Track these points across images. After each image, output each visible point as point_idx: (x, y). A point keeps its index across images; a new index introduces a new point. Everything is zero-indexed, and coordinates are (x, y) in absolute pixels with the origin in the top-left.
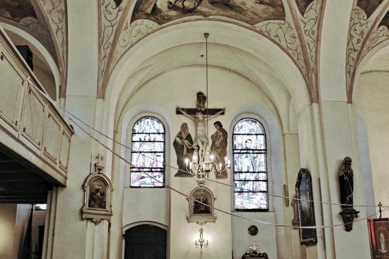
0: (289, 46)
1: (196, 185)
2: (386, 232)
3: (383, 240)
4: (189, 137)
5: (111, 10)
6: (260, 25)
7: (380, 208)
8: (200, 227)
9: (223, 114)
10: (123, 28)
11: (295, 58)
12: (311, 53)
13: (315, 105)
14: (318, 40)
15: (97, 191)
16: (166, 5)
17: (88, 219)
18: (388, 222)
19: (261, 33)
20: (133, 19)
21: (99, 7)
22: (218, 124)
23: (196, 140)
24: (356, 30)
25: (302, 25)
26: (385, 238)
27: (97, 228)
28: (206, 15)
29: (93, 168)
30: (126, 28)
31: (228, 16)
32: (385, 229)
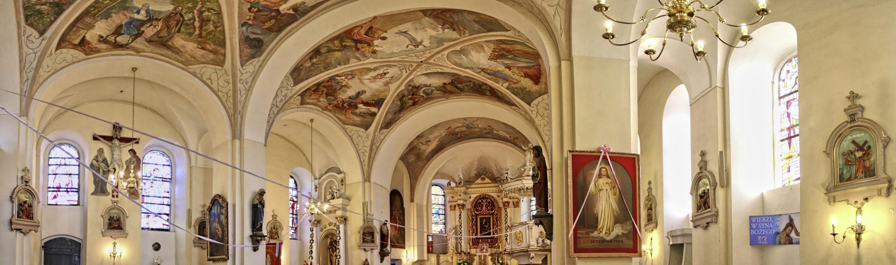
0: (221, 89)
1: (110, 204)
4: (105, 161)
5: (34, 39)
6: (192, 68)
8: (113, 241)
9: (137, 143)
10: (47, 55)
11: (224, 100)
12: (240, 98)
13: (237, 142)
14: (249, 90)
15: (25, 202)
16: (97, 38)
17: (17, 230)
19: (194, 74)
20: (57, 49)
21: (19, 37)
22: (132, 151)
23: (112, 163)
25: (239, 74)
27: (25, 238)
28: (138, 51)
29: (19, 180)
30: (51, 55)
31: (162, 55)
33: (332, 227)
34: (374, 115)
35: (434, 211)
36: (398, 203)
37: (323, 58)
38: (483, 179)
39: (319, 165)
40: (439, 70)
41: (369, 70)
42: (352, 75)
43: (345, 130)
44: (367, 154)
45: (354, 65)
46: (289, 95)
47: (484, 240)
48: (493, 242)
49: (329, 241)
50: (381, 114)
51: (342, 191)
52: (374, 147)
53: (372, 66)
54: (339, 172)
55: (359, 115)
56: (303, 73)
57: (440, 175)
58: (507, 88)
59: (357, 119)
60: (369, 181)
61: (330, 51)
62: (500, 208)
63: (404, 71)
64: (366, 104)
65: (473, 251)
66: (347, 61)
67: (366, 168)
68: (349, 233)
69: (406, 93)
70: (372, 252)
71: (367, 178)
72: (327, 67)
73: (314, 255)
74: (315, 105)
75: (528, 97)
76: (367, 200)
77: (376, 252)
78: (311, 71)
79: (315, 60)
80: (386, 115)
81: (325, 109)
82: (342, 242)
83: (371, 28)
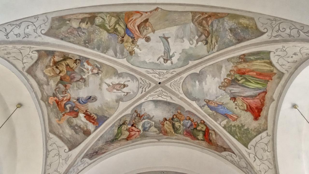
24: (28, 28)
34: (87, 133)
37: (91, 29)
40: (169, 100)
41: (116, 73)
42: (99, 68)
43: (46, 140)
45: (105, 58)
46: (31, 39)
50: (98, 134)
53: (120, 70)
55: (73, 127)
56: (64, 29)
58: (225, 127)
59: (68, 131)
61: (102, 26)
63: (140, 90)
64: (88, 116)
66: (105, 50)
69: (128, 120)
72: (87, 43)
74: (40, 85)
75: (245, 137)
78: (72, 33)
79: (83, 25)
80: (99, 140)
81: (45, 99)
83: (147, 20)
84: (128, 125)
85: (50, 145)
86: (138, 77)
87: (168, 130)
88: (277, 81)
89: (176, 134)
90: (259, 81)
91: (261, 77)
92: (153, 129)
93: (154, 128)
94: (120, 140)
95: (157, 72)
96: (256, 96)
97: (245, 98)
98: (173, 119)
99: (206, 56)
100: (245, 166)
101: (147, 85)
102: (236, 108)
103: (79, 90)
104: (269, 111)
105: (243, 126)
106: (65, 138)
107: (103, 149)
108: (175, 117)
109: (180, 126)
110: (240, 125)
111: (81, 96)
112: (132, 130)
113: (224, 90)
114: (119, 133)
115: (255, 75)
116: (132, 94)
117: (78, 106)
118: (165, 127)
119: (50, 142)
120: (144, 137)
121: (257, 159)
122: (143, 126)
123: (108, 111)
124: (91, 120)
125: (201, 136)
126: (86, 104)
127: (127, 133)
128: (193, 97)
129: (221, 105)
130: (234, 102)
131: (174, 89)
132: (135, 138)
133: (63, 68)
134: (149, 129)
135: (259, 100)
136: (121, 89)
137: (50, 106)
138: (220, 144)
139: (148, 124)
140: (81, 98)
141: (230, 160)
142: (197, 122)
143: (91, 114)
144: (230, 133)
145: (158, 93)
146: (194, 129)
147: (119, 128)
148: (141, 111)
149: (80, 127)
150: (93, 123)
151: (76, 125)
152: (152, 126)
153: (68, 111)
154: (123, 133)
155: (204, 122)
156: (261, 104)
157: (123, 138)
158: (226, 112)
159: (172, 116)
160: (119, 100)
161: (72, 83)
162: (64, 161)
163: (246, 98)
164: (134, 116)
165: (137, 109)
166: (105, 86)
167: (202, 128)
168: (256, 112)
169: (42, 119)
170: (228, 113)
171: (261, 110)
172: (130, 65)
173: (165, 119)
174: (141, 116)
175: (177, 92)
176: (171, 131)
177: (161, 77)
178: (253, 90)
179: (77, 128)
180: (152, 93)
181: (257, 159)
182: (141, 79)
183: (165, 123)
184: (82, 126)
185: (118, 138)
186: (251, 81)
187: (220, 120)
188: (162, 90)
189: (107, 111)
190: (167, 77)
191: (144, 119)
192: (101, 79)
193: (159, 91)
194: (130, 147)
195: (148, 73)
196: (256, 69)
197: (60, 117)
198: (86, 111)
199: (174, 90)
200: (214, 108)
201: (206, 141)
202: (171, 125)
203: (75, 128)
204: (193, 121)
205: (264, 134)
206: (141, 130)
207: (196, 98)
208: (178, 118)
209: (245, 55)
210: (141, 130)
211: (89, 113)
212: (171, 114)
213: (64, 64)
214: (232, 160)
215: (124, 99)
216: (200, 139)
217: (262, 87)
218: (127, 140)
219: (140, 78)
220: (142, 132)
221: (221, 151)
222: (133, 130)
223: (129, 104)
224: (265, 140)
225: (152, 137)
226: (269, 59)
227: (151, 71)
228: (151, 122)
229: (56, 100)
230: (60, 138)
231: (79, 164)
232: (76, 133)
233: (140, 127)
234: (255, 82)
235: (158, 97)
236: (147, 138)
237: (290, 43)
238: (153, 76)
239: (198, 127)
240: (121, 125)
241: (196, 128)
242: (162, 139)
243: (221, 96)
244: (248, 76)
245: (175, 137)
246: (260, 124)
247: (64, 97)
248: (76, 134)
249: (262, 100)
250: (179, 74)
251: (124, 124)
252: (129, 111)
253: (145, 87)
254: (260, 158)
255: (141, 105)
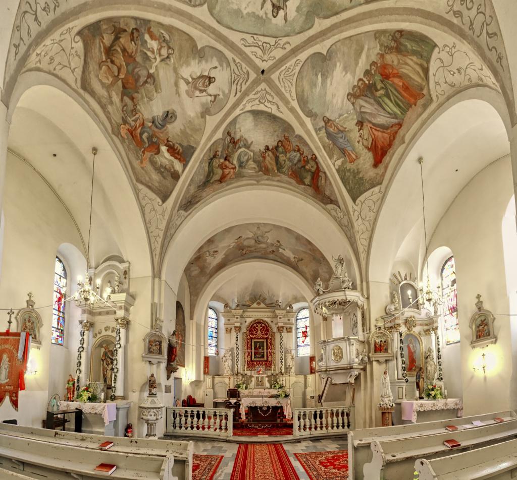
2: (13, 353)
3: (5, 365)
7: (10, 317)
18: (19, 339)
26: (9, 361)
32: (12, 349)
33: (109, 333)
35: (209, 333)
36: (181, 317)
38: (259, 304)
39: (97, 249)
40: (275, 112)
44: (160, 240)
47: (260, 363)
48: (268, 364)
49: (103, 350)
51: (125, 286)
52: (169, 234)
53: (203, 39)
54: (122, 261)
57: (216, 297)
60: (160, 278)
62: (274, 333)
63: (234, 87)
64: (172, 150)
65: (248, 373)
67: (156, 260)
68: (131, 339)
70: (158, 367)
71: (157, 274)
73: (83, 368)
76: (156, 300)
77: (163, 365)
80: (190, 185)
82: (120, 356)
84: (220, 158)
85: (143, 199)
86: (229, 55)
87: (270, 167)
88: (420, 110)
89: (279, 174)
90: (401, 101)
91: (405, 95)
92: (252, 164)
93: (252, 163)
94: (212, 183)
95: (260, 43)
96: (387, 128)
97: (374, 127)
98: (277, 148)
99: (346, 10)
100: (347, 224)
101: (243, 76)
102: (359, 142)
103: (151, 102)
104: (392, 159)
105: (359, 173)
106: (155, 187)
107: (196, 196)
108: (280, 145)
109: (285, 161)
110: (356, 171)
111: (155, 115)
112: (226, 166)
113: (353, 104)
114: (210, 173)
115: (399, 86)
116: (222, 98)
117: (157, 135)
118: (267, 161)
119: (141, 196)
120: (240, 177)
121: (360, 219)
122: (239, 159)
123: (194, 136)
124: (176, 155)
125: (308, 180)
126: (165, 128)
127: (220, 172)
128: (308, 108)
129: (342, 132)
130: (360, 130)
131: (283, 87)
132: (230, 178)
133: (120, 59)
134: (246, 165)
135: (388, 136)
136: (206, 89)
137: (125, 142)
138: (327, 193)
139: (245, 155)
140: (156, 119)
141: (333, 214)
142: (307, 156)
143: (174, 145)
144: (342, 179)
145: (259, 95)
146: (302, 167)
147: (210, 163)
148: (236, 131)
149: (165, 168)
150: (180, 160)
151: (161, 166)
152: (250, 159)
153: (147, 145)
154: (215, 172)
155: (316, 158)
156: (388, 143)
157: (216, 179)
158: (346, 146)
159: (277, 143)
160: (206, 112)
161: (139, 89)
162: (161, 216)
163: (375, 128)
164: (227, 143)
165: (230, 128)
166: (183, 87)
167: (312, 167)
168: (380, 153)
169: (118, 154)
170: (347, 149)
171: (386, 152)
172: (215, 25)
173: (267, 148)
174: (236, 143)
175: (287, 95)
176: (273, 169)
177: (266, 58)
178: (389, 116)
179: (163, 170)
180: (251, 96)
181: (360, 219)
182: (234, 61)
183: (267, 154)
184: (167, 167)
185: (210, 180)
186: (392, 98)
187: (335, 157)
188: (265, 89)
189: (192, 136)
190: (275, 58)
191: (240, 148)
192: (175, 70)
193: (262, 90)
194: (224, 193)
195: (246, 46)
196: (405, 73)
197: (140, 157)
198: (168, 141)
199: (283, 90)
200: (333, 134)
201: (313, 188)
202: (273, 158)
203: (161, 170)
204: (303, 154)
205: (376, 189)
206: (237, 166)
207: (313, 111)
208: (284, 147)
209: (403, 33)
210: (237, 166)
211: (171, 143)
212: (276, 138)
213: (119, 50)
214: (336, 215)
215: (212, 110)
216: (306, 183)
217: (400, 113)
218: (221, 182)
219: (233, 58)
220: (237, 169)
221: (326, 204)
222: (227, 167)
223: (220, 118)
224: (375, 198)
225: (251, 177)
226: (428, 61)
227: (250, 39)
228: (249, 152)
229: (128, 130)
230: (149, 187)
231: (176, 218)
232: (164, 178)
233: (235, 162)
234: (395, 101)
235: (259, 103)
236: (244, 178)
237: (463, 43)
238: (252, 52)
239: (307, 165)
240: (211, 159)
241: (304, 167)
242: (262, 180)
243: (346, 115)
244: (390, 85)
245: (278, 178)
246: (377, 174)
247: (135, 121)
248: (164, 180)
249: (392, 138)
250: (295, 51)
251: (215, 156)
252: (219, 135)
253: (240, 82)
254: (364, 217)
255: (234, 121)
